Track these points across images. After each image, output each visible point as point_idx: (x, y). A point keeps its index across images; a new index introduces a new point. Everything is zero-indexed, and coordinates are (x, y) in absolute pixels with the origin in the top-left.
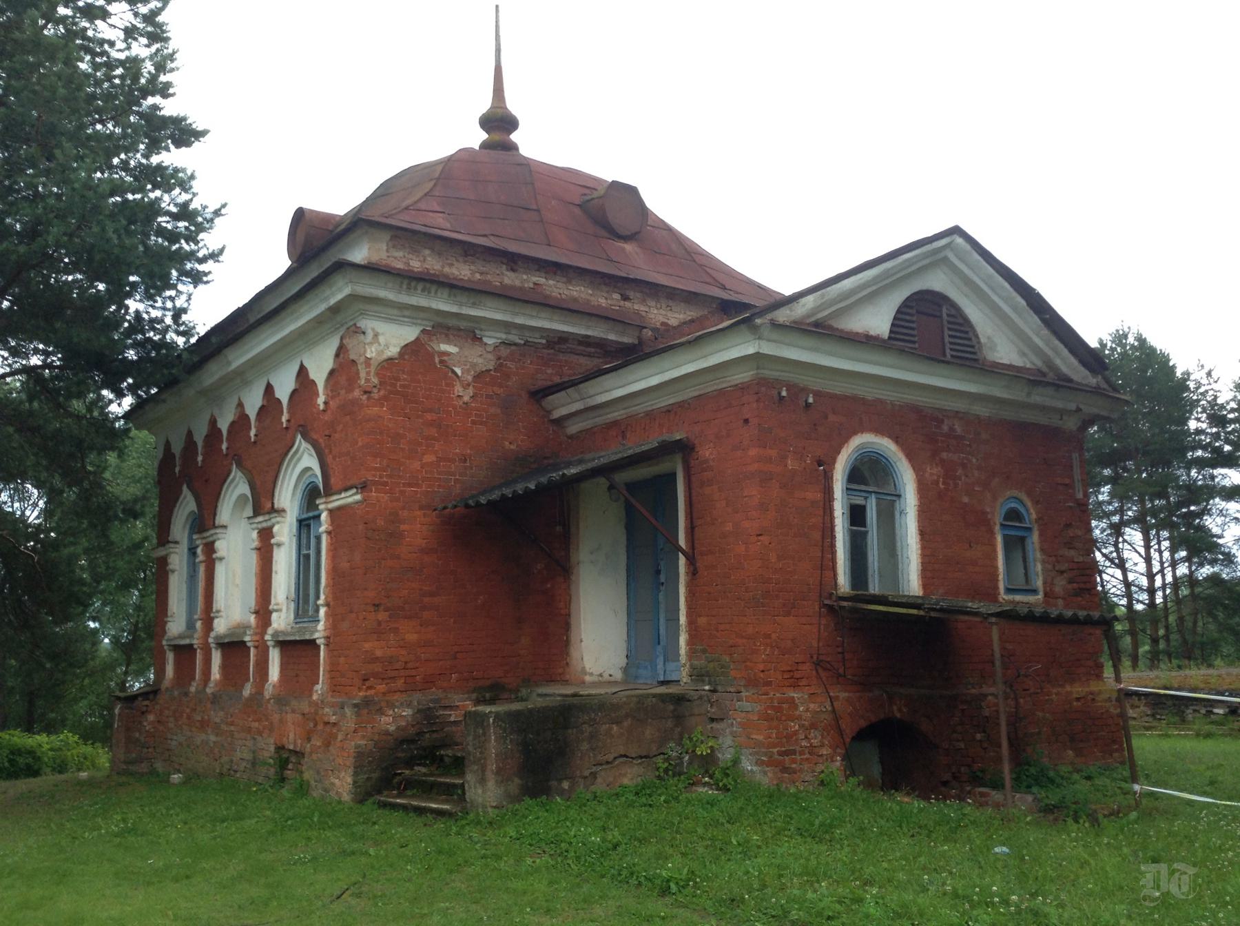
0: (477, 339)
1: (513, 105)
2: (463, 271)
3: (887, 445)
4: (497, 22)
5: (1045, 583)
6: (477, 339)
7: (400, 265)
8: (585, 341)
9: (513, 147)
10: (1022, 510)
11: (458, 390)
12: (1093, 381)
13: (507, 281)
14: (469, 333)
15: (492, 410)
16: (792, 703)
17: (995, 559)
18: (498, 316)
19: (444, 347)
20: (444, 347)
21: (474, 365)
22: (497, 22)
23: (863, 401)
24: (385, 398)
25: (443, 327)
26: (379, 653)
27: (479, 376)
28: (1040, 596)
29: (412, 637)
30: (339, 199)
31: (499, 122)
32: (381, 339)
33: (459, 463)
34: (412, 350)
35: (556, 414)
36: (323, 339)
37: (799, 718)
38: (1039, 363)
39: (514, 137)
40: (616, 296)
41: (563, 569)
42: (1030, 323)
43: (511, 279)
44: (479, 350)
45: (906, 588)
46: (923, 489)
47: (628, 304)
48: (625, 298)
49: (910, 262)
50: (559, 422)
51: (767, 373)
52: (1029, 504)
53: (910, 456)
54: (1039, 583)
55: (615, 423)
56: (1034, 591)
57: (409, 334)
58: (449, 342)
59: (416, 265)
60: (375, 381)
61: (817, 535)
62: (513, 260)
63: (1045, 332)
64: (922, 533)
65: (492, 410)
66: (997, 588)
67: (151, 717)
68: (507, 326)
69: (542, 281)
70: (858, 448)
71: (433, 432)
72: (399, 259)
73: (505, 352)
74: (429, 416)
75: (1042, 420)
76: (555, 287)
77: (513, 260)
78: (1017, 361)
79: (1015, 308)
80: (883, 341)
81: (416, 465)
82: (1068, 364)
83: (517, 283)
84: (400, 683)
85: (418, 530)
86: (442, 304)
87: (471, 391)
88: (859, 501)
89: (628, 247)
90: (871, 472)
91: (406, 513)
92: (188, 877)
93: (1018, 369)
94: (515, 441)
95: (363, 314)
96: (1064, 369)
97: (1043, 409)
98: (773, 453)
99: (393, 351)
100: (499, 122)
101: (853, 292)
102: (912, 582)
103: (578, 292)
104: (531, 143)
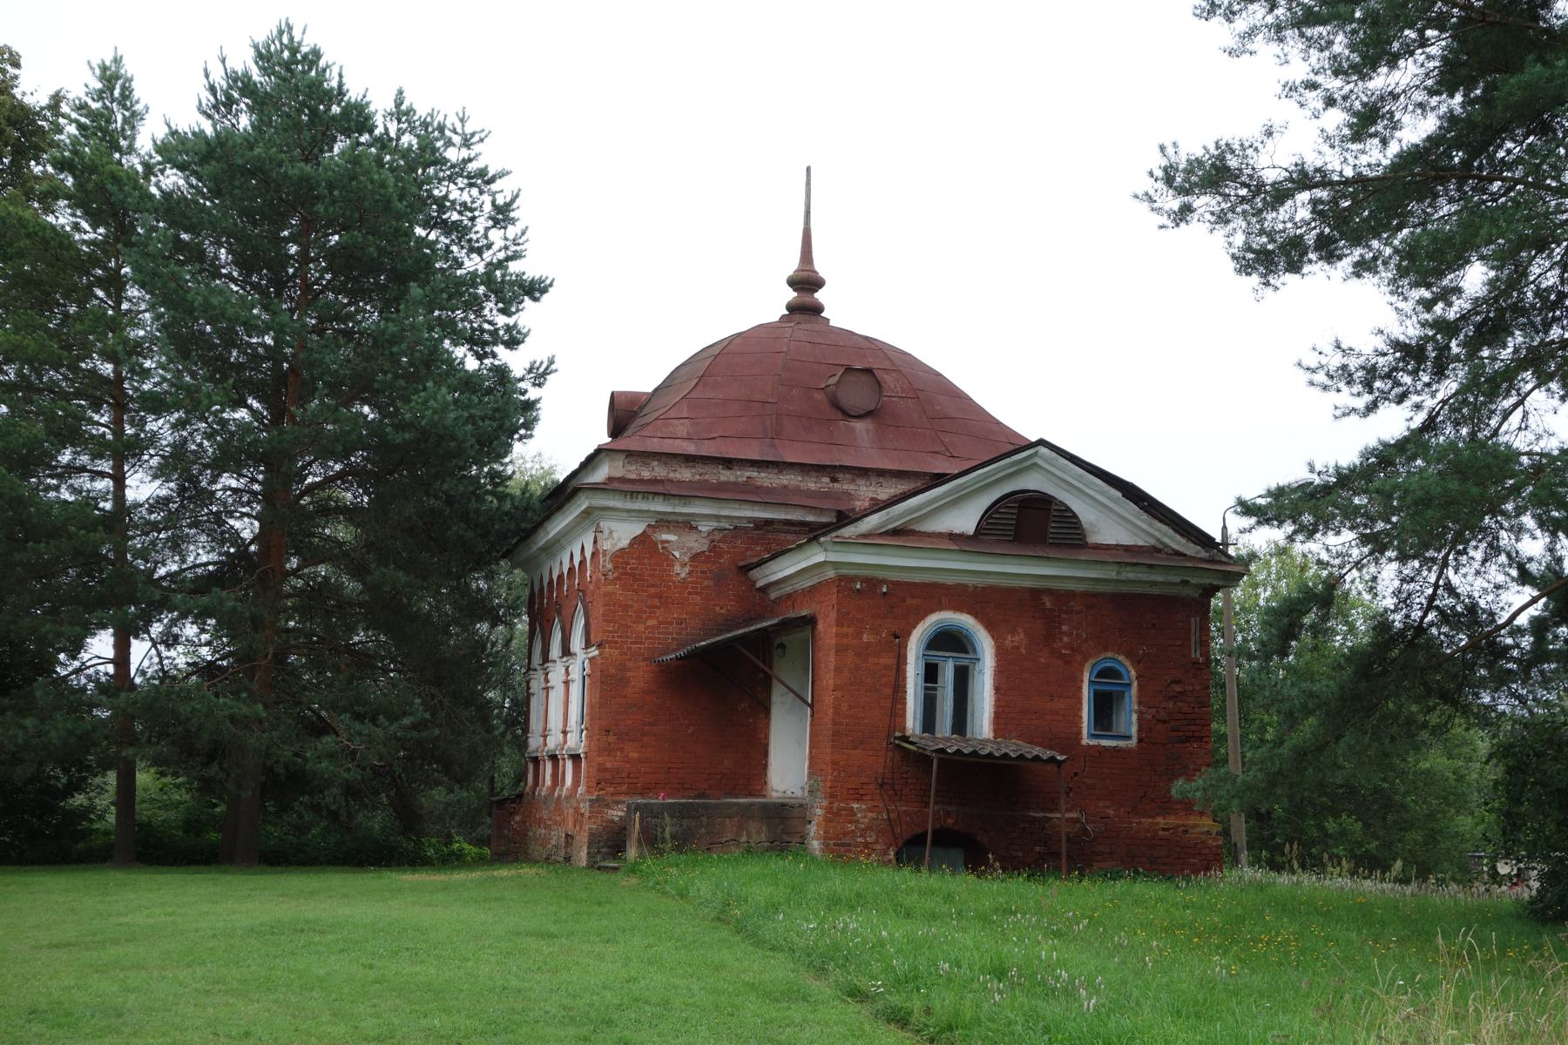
0: (694, 528)
1: (821, 266)
2: (685, 474)
3: (965, 621)
4: (808, 184)
5: (1139, 731)
6: (694, 528)
7: (633, 476)
8: (780, 521)
9: (817, 309)
10: (1121, 669)
11: (677, 568)
12: (1203, 554)
13: (723, 478)
14: (687, 525)
15: (706, 583)
16: (851, 812)
17: (1080, 709)
18: (706, 511)
19: (665, 537)
20: (665, 537)
21: (690, 549)
22: (808, 184)
23: (944, 587)
24: (618, 578)
25: (664, 522)
26: (608, 765)
27: (695, 557)
28: (1133, 742)
29: (635, 755)
30: (645, 382)
31: (806, 282)
32: (615, 535)
33: (675, 630)
34: (641, 541)
35: (760, 584)
36: (585, 530)
37: (857, 821)
38: (1153, 542)
39: (820, 295)
40: (826, 480)
41: (763, 709)
42: (1130, 509)
43: (726, 476)
44: (695, 536)
45: (977, 729)
46: (1001, 653)
47: (837, 485)
48: (834, 480)
49: (987, 476)
50: (764, 589)
51: (844, 572)
52: (1128, 664)
53: (990, 627)
54: (1134, 730)
55: (789, 596)
56: (1129, 738)
57: (637, 528)
58: (669, 532)
59: (646, 474)
60: (610, 566)
61: (889, 691)
62: (728, 463)
63: (1145, 516)
64: (997, 689)
65: (706, 583)
66: (1080, 733)
67: (518, 818)
68: (718, 518)
69: (755, 474)
70: (937, 622)
71: (656, 602)
72: (634, 471)
73: (718, 536)
74: (652, 590)
75: (1156, 591)
76: (765, 478)
77: (728, 463)
78: (1126, 538)
79: (1111, 499)
80: (968, 537)
81: (641, 628)
82: (1177, 542)
83: (732, 479)
84: (624, 788)
85: (640, 677)
86: (660, 506)
87: (687, 569)
88: (933, 660)
89: (859, 426)
90: (949, 641)
91: (631, 664)
92: (518, 934)
93: (1127, 549)
94: (724, 607)
95: (602, 518)
96: (1176, 547)
97: (1154, 584)
98: (850, 630)
99: (625, 543)
100: (806, 282)
101: (919, 507)
102: (983, 723)
103: (789, 479)
104: (844, 309)
